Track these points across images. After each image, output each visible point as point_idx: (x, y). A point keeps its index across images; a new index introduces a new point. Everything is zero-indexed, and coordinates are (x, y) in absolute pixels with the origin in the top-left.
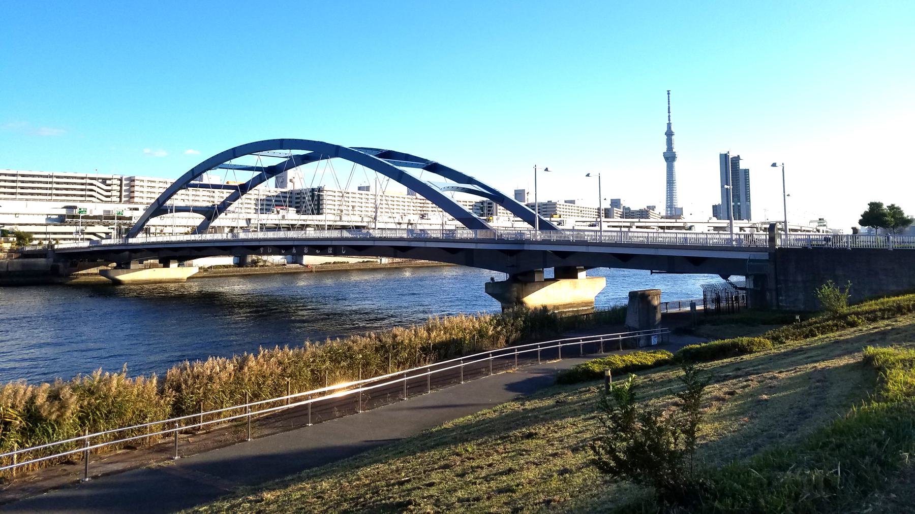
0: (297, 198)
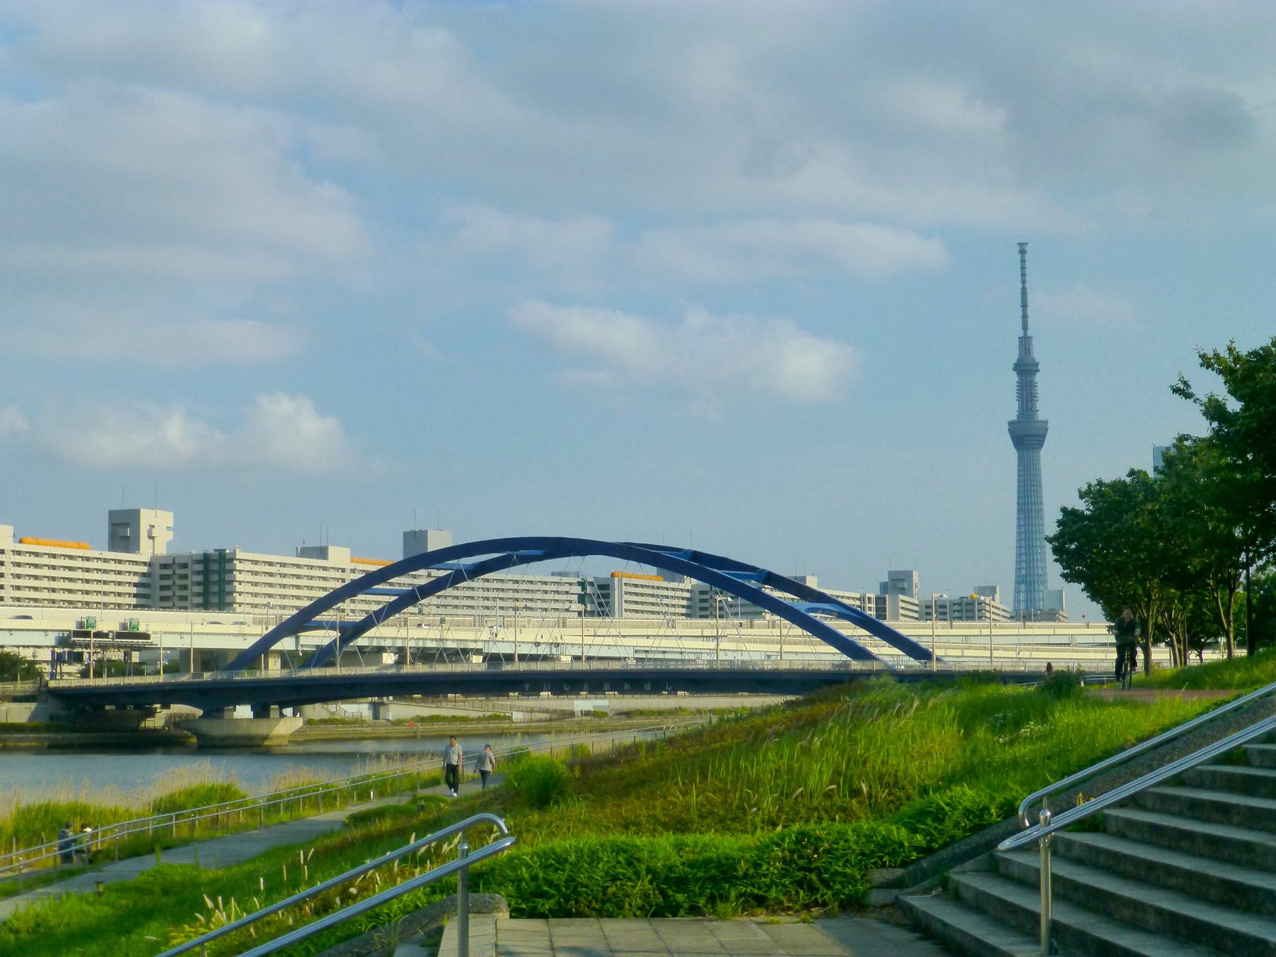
0: (163, 588)
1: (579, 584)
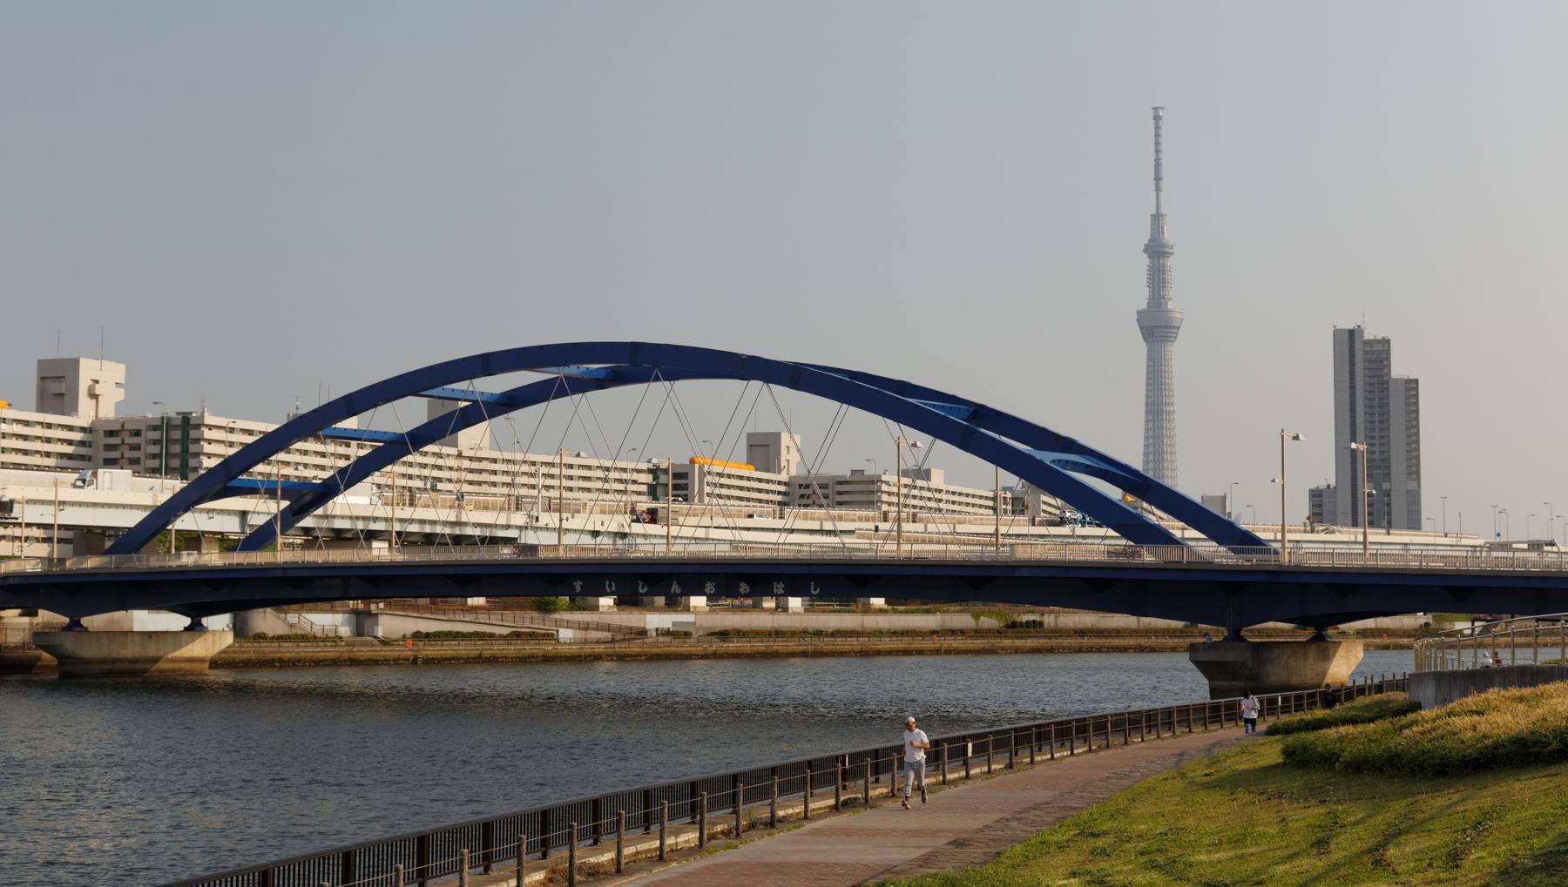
1: (650, 471)
